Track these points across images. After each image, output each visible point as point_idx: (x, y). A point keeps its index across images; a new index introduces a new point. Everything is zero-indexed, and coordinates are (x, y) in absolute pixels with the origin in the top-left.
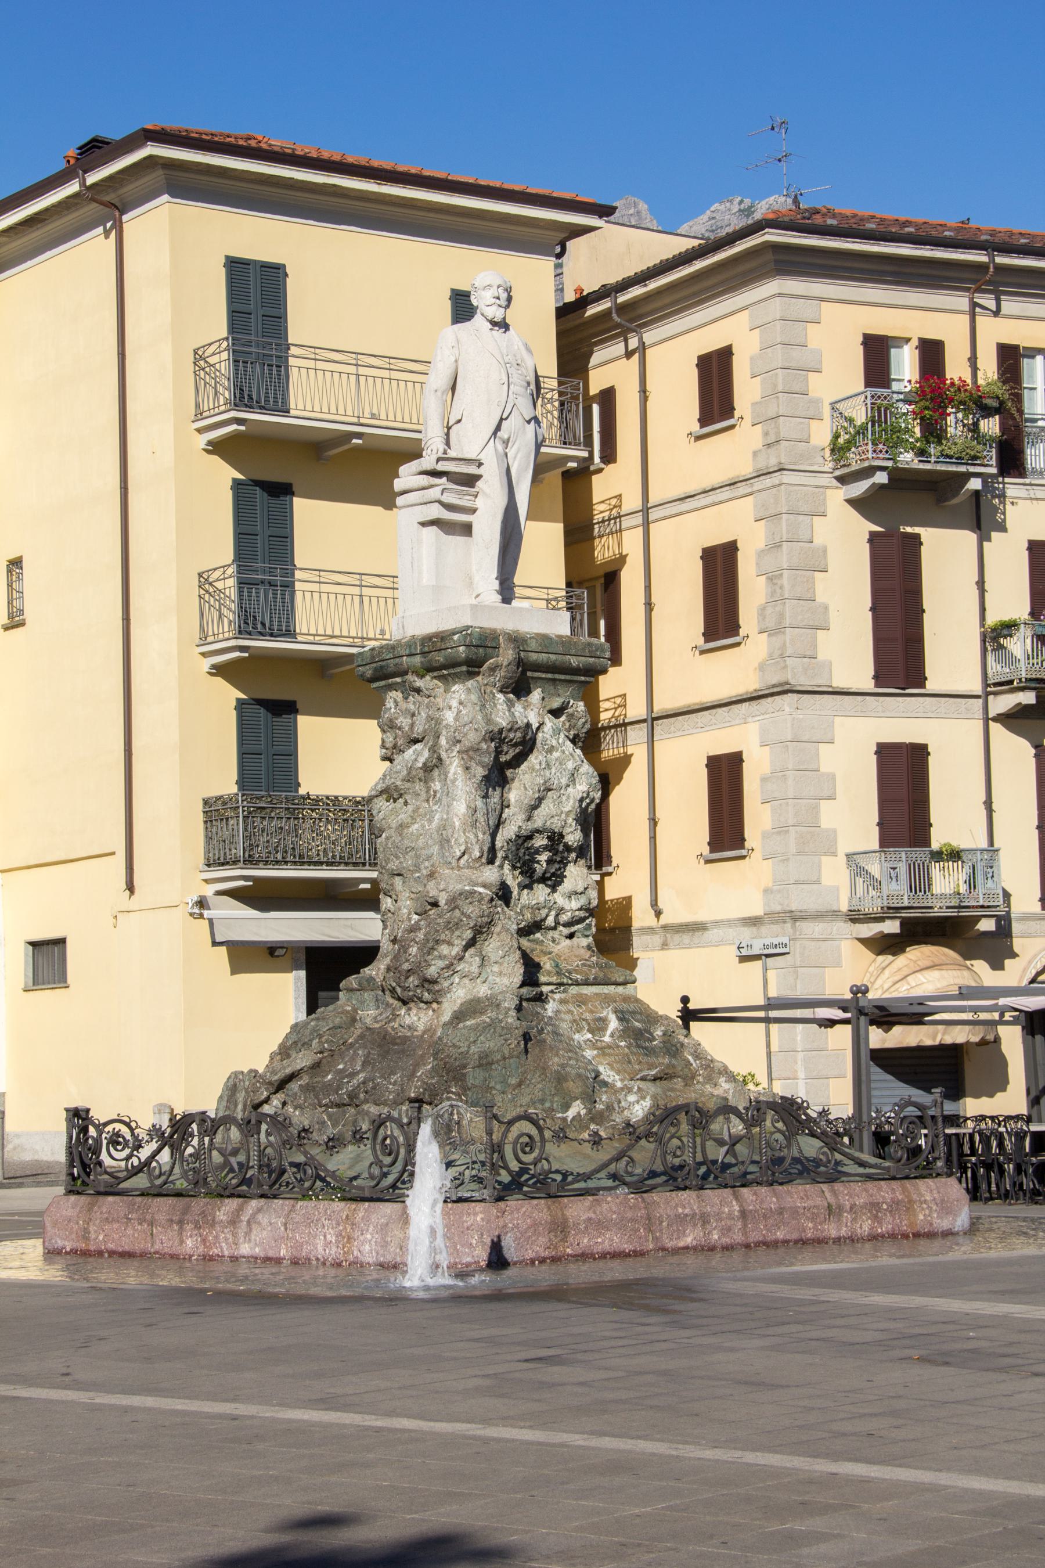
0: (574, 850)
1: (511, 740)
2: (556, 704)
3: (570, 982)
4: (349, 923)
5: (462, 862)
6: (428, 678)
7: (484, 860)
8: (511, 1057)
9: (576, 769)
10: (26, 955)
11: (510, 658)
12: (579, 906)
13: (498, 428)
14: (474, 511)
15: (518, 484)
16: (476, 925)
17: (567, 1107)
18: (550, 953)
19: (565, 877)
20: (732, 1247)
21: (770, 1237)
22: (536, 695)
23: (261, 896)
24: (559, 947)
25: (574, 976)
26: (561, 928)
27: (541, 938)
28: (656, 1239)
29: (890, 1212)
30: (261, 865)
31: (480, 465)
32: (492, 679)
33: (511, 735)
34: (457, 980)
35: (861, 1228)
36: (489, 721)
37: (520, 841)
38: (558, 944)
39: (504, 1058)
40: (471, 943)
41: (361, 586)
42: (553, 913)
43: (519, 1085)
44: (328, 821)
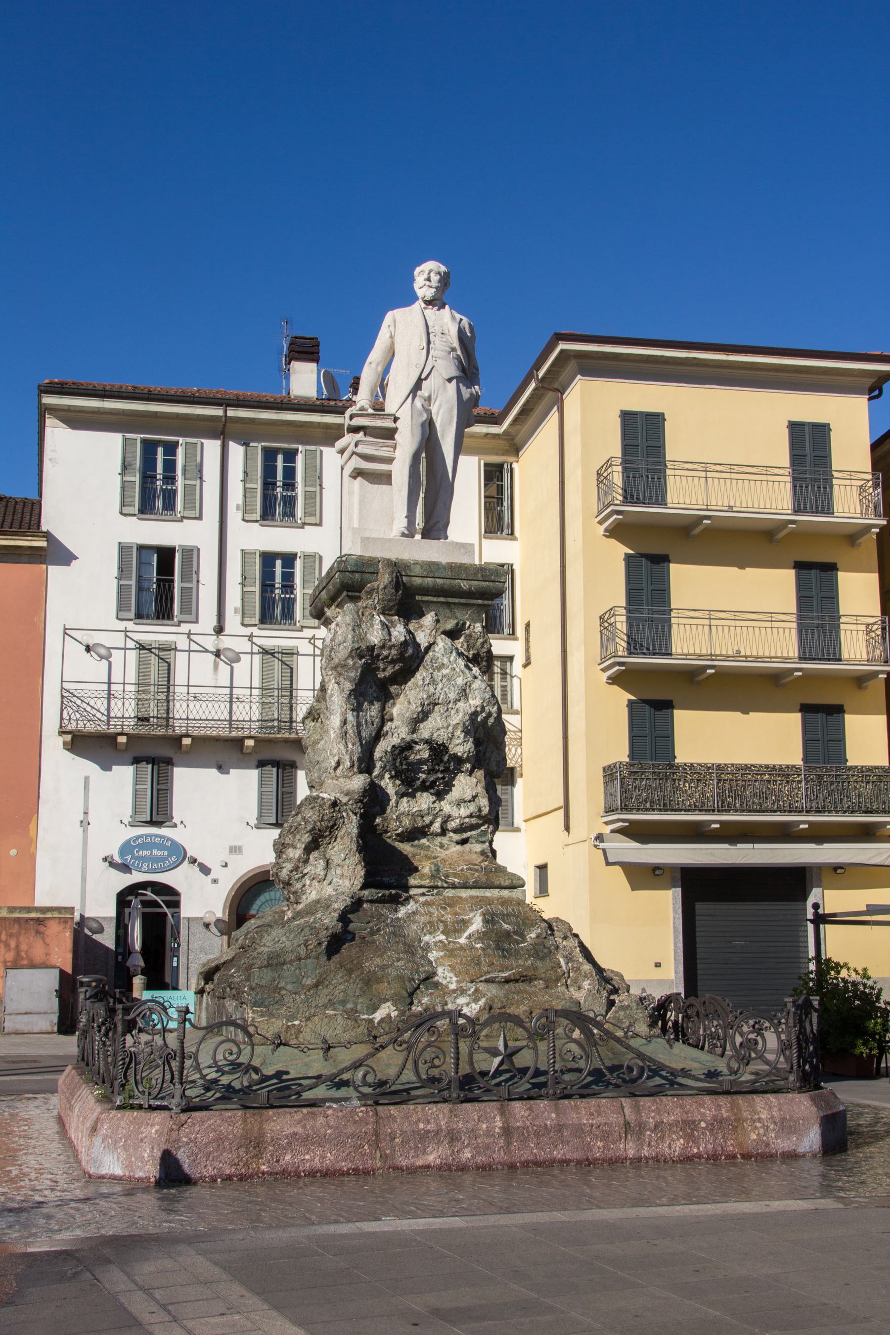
0: (467, 760)
1: (386, 657)
2: (450, 625)
3: (445, 885)
4: (709, 851)
5: (339, 771)
6: (333, 607)
7: (355, 770)
8: (307, 957)
9: (468, 685)
10: (535, 875)
11: (386, 581)
12: (468, 813)
13: (418, 386)
14: (390, 461)
15: (443, 436)
16: (313, 829)
17: (375, 1009)
18: (435, 858)
19: (454, 786)
20: (490, 1167)
21: (542, 1156)
22: (429, 619)
23: (638, 832)
24: (447, 852)
25: (451, 879)
26: (451, 834)
27: (428, 843)
28: (384, 1157)
29: (711, 1131)
30: (634, 812)
31: (396, 420)
32: (370, 602)
33: (385, 653)
34: (308, 882)
35: (670, 1147)
36: (362, 638)
37: (397, 752)
38: (447, 849)
39: (299, 959)
40: (313, 846)
41: (710, 619)
42: (439, 820)
43: (316, 985)
44: (686, 781)
